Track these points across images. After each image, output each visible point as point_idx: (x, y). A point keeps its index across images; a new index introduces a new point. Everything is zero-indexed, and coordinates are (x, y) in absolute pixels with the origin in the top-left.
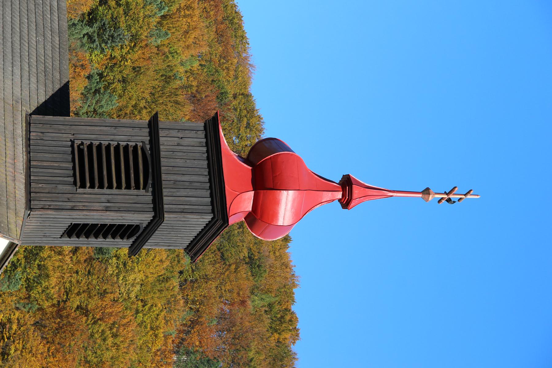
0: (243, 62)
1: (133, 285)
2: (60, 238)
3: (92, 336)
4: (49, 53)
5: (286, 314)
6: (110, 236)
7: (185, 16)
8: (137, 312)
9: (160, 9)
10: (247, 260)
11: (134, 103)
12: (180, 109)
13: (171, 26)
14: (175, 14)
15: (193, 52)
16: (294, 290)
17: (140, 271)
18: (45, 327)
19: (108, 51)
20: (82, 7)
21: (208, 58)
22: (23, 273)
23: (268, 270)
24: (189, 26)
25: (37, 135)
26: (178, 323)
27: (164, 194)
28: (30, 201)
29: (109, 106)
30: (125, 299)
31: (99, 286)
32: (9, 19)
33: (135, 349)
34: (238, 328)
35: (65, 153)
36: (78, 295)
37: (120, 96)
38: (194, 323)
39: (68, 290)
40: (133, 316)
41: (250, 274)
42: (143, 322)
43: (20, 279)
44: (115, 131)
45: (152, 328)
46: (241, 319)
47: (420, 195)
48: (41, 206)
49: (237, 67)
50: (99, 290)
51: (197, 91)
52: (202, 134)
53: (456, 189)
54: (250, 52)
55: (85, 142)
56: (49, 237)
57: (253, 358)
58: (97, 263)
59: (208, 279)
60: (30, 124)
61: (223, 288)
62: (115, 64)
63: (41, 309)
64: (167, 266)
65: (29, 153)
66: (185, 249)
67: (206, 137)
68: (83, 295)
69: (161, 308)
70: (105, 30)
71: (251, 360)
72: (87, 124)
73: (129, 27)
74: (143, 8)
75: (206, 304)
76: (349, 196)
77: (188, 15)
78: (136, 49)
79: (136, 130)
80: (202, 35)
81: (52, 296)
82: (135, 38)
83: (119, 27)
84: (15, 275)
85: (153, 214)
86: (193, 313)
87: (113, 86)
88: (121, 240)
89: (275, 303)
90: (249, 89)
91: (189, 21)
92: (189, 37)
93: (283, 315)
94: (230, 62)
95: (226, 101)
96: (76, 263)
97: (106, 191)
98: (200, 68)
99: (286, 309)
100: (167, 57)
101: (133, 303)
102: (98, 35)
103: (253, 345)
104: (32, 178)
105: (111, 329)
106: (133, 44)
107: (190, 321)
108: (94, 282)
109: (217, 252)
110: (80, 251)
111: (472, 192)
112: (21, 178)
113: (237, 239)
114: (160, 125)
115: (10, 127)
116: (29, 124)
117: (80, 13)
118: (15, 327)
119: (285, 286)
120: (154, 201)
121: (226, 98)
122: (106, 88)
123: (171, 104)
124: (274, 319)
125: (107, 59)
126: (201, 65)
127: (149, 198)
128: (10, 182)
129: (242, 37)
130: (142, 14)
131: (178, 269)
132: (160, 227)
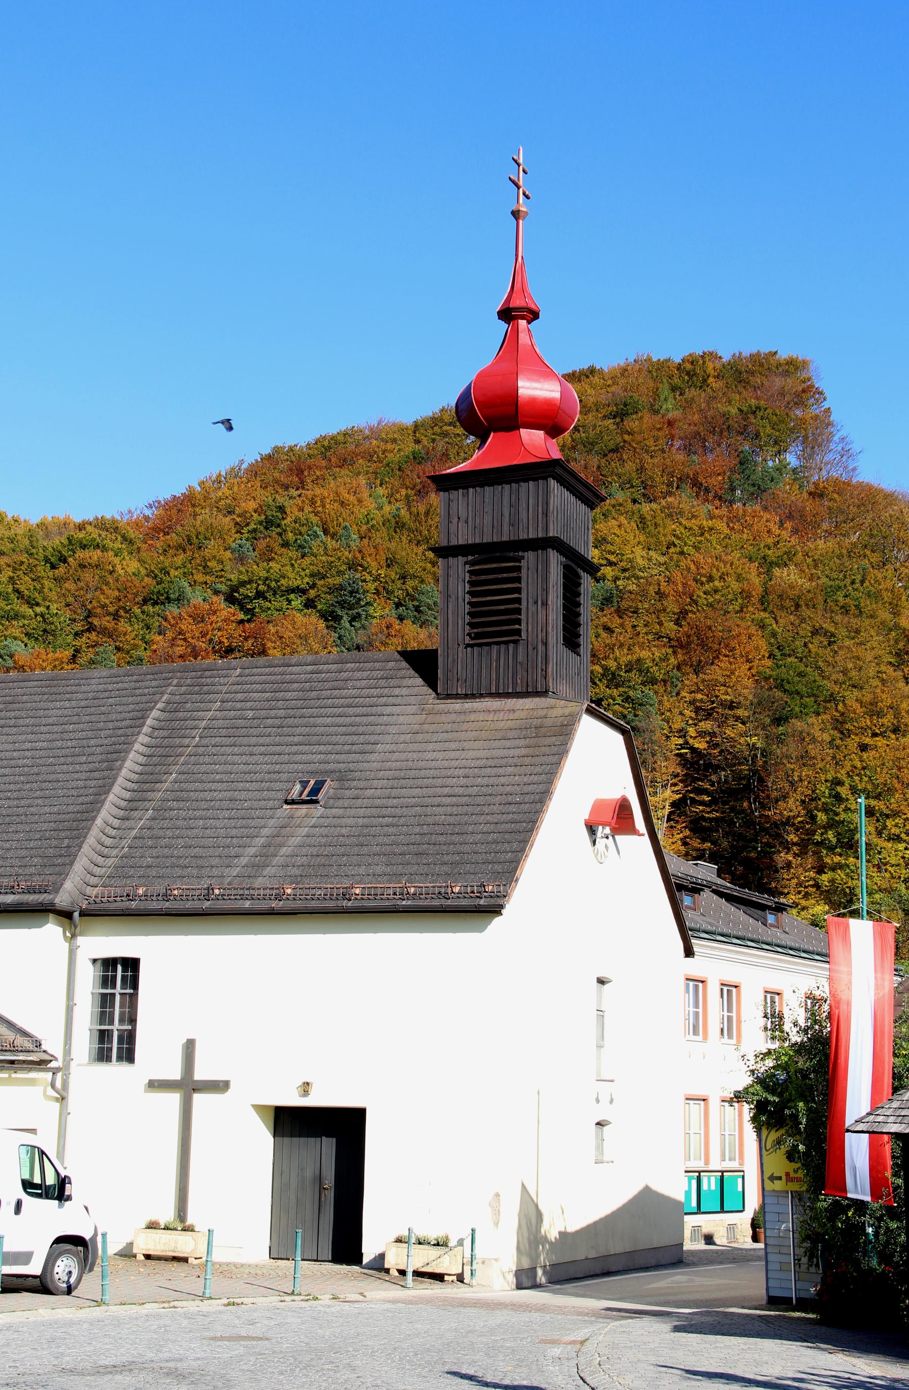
0: (375, 433)
1: (650, 560)
2: (580, 656)
3: (710, 605)
4: (365, 674)
5: (684, 368)
6: (578, 599)
7: (324, 506)
8: (682, 553)
9: (316, 536)
10: (618, 420)
11: (429, 565)
12: (435, 509)
13: (335, 522)
14: (320, 517)
15: (365, 495)
16: (655, 359)
17: (633, 552)
18: (700, 661)
19: (370, 597)
20: (319, 628)
21: (372, 476)
22: (636, 690)
23: (630, 394)
24: (335, 501)
25: (461, 686)
26: (695, 503)
27: (525, 537)
28: (537, 692)
29: (434, 595)
30: (666, 569)
31: (651, 600)
32: (329, 720)
33: (727, 554)
34: (702, 429)
35: (480, 655)
36: (663, 624)
37: (422, 581)
38: (696, 484)
39: (657, 636)
40: (685, 558)
41: (634, 416)
42: (695, 547)
43: (643, 692)
44: (454, 597)
45: (702, 535)
46: (690, 425)
47: (521, 222)
48: (543, 680)
49: (382, 440)
50: (655, 600)
51: (412, 489)
52: (454, 494)
53: (512, 177)
54: (363, 425)
55: (467, 631)
56: (579, 669)
57: (738, 408)
58: (623, 603)
59: (642, 467)
60: (448, 695)
61: (653, 448)
62: (384, 588)
63: (679, 668)
64: (626, 519)
65: (481, 696)
66: (592, 509)
67: (456, 489)
68: (663, 619)
69: (677, 524)
70: (345, 602)
71: (740, 410)
72: (446, 630)
73: (340, 573)
74: (316, 557)
75: (672, 470)
76: (524, 312)
77: (322, 501)
78: (366, 565)
79: (451, 572)
80: (345, 484)
81: (663, 655)
82: (353, 566)
83: (340, 585)
84: (638, 698)
85: (550, 551)
86: (684, 485)
87: (410, 590)
88: (582, 585)
89: (670, 383)
90: (408, 424)
91: (328, 501)
92: (348, 501)
93: (685, 373)
94: (376, 449)
95: (423, 452)
96: (623, 628)
97: (523, 606)
98: (384, 486)
99: (678, 369)
100: (373, 526)
101: (671, 559)
102: (350, 609)
103: (722, 408)
104: (510, 691)
105: (702, 584)
106: (360, 568)
107: (693, 487)
108: (646, 606)
109: (608, 458)
110: (609, 624)
111: (515, 157)
112: (511, 703)
113: (592, 433)
114: (444, 543)
115: (453, 717)
116: (448, 696)
117: (325, 631)
118: (699, 696)
119: (650, 372)
120: (535, 549)
121: (420, 453)
122: (413, 599)
123: (429, 520)
124: (690, 383)
125: (379, 598)
126: (381, 485)
127: (530, 556)
128: (516, 715)
129: (345, 435)
130: (324, 558)
131: (630, 505)
132: (565, 541)
